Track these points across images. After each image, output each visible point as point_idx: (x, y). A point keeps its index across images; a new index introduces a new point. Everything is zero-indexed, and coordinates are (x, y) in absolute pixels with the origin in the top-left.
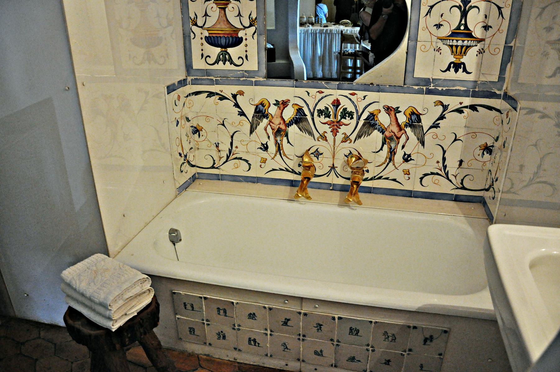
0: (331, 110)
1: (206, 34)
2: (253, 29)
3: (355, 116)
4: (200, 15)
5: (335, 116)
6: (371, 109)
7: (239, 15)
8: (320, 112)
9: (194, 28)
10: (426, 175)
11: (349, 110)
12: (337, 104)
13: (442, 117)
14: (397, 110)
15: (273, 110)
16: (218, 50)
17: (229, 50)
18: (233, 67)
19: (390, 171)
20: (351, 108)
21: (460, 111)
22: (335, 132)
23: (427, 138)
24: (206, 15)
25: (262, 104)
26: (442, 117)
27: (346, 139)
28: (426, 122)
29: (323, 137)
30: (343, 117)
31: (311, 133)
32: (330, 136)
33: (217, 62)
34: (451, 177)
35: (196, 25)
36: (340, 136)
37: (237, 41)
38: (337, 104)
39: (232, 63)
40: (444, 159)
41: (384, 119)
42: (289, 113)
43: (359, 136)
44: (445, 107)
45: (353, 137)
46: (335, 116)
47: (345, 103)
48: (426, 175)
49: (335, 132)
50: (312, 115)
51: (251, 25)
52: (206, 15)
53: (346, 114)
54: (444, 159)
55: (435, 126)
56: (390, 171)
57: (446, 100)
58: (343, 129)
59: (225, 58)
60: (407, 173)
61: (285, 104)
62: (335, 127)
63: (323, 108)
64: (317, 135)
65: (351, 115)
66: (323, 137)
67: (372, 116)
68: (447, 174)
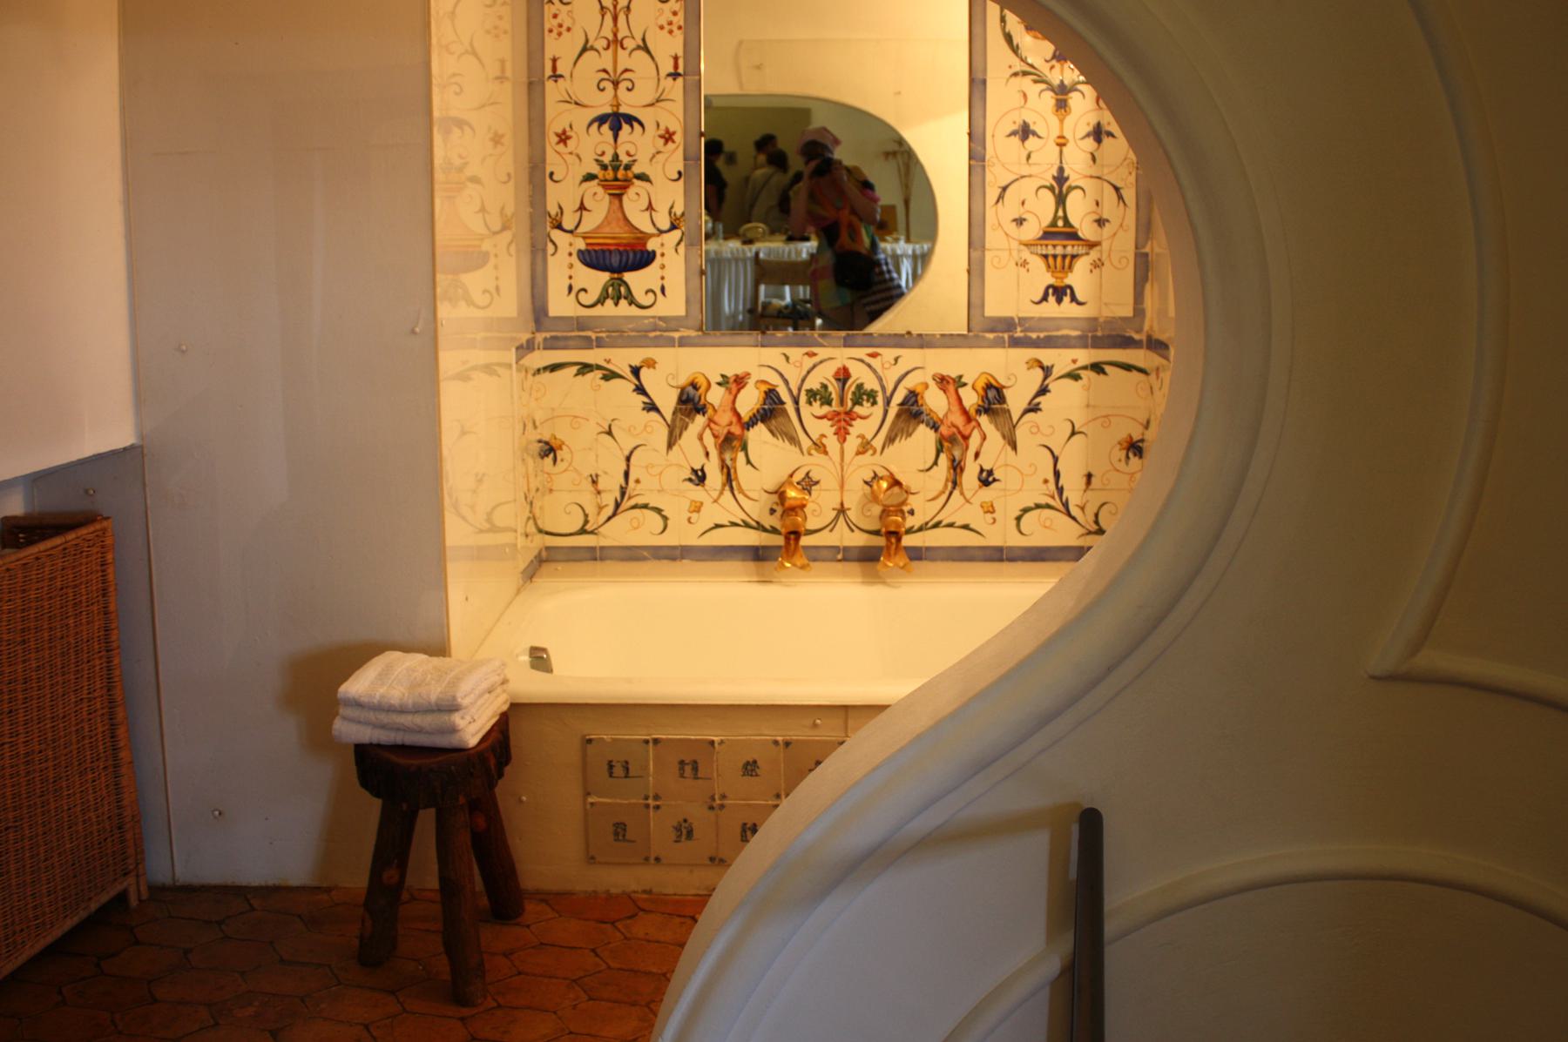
0: (833, 389)
1: (581, 244)
2: (677, 234)
3: (880, 399)
4: (570, 206)
5: (842, 401)
6: (909, 383)
7: (650, 207)
8: (812, 395)
9: (556, 235)
10: (1026, 510)
11: (868, 387)
12: (843, 376)
13: (1043, 391)
14: (959, 383)
15: (716, 396)
16: (605, 277)
17: (629, 277)
18: (634, 311)
19: (957, 510)
20: (871, 384)
21: (1074, 376)
22: (842, 434)
23: (1021, 434)
24: (582, 208)
25: (694, 386)
26: (1043, 391)
27: (865, 447)
28: (1016, 401)
29: (820, 447)
30: (857, 401)
31: (794, 440)
32: (832, 443)
33: (601, 301)
34: (1074, 511)
35: (559, 227)
36: (852, 443)
37: (643, 259)
38: (843, 376)
39: (632, 302)
40: (1057, 474)
41: (936, 401)
42: (749, 401)
43: (890, 439)
44: (1047, 371)
45: (878, 443)
46: (842, 401)
47: (860, 374)
48: (1026, 510)
49: (842, 434)
50: (796, 402)
51: (673, 227)
52: (582, 208)
53: (863, 395)
54: (1057, 474)
55: (1033, 408)
56: (957, 510)
57: (1047, 356)
58: (858, 428)
59: (617, 292)
60: (990, 509)
61: (740, 381)
62: (843, 422)
63: (816, 386)
64: (806, 443)
65: (872, 396)
66: (820, 447)
67: (913, 397)
68: (1066, 505)
